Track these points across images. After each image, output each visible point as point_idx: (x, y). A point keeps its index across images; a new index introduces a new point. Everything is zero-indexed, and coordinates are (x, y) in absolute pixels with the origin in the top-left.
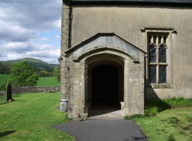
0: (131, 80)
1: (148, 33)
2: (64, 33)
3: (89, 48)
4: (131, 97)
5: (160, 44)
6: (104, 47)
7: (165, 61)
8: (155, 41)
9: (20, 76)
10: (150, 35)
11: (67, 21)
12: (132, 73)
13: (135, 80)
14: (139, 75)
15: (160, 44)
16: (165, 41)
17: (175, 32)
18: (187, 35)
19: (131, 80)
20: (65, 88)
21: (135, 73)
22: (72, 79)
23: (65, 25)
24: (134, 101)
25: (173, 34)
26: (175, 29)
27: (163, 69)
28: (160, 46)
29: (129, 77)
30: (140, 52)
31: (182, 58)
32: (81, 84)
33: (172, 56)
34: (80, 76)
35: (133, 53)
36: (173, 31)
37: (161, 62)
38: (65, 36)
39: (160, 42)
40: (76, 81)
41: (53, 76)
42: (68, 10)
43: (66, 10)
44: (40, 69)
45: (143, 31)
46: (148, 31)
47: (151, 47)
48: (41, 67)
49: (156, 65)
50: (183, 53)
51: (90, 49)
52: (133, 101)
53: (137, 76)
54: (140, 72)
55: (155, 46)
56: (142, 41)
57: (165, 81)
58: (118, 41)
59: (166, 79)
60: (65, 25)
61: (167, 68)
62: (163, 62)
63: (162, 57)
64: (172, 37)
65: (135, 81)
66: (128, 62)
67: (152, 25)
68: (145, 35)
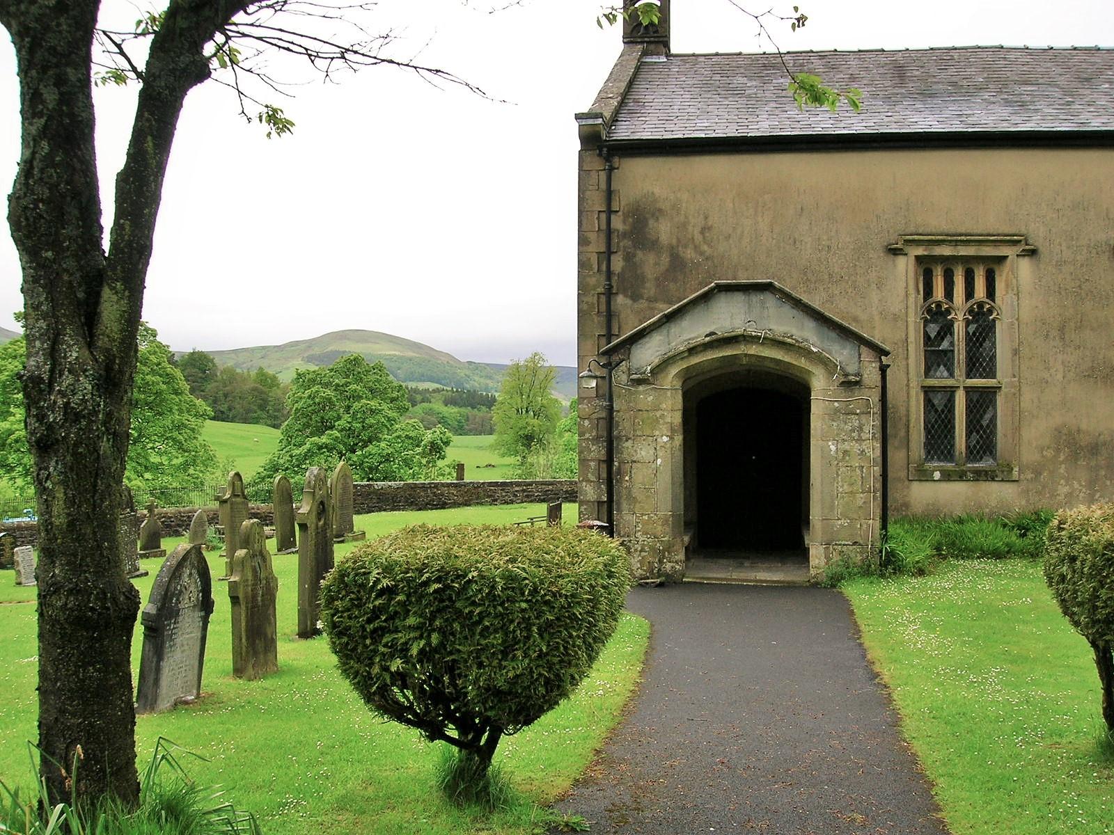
0: (833, 448)
1: (918, 258)
2: (591, 268)
3: (686, 336)
4: (832, 508)
5: (969, 304)
6: (739, 332)
7: (991, 374)
8: (949, 294)
9: (336, 433)
10: (926, 265)
11: (598, 218)
12: (835, 424)
13: (846, 446)
14: (861, 429)
15: (969, 304)
16: (991, 292)
17: (1032, 253)
18: (1082, 265)
19: (833, 448)
20: (593, 478)
21: (846, 423)
22: (629, 444)
23: (592, 236)
24: (845, 522)
25: (1025, 265)
26: (1030, 241)
27: (982, 401)
28: (971, 311)
29: (825, 438)
30: (864, 349)
31: (1060, 357)
32: (659, 461)
33: (1016, 352)
34: (657, 433)
35: (842, 354)
36: (1023, 250)
37: (975, 377)
38: (592, 281)
39: (969, 293)
40: (643, 451)
41: (491, 432)
42: (603, 175)
43: (594, 175)
44: (416, 391)
45: (894, 252)
46: (920, 251)
47: (937, 316)
48: (422, 378)
49: (951, 391)
50: (1063, 339)
51: (690, 339)
52: (839, 522)
53: (855, 435)
54: (864, 419)
55: (948, 311)
56: (890, 303)
57: (991, 453)
58: (788, 310)
59: (995, 446)
60: (592, 236)
61: (1000, 400)
62: (981, 377)
63: (980, 361)
64: (1020, 274)
65: (845, 452)
66: (820, 385)
67: (937, 223)
68: (905, 267)
